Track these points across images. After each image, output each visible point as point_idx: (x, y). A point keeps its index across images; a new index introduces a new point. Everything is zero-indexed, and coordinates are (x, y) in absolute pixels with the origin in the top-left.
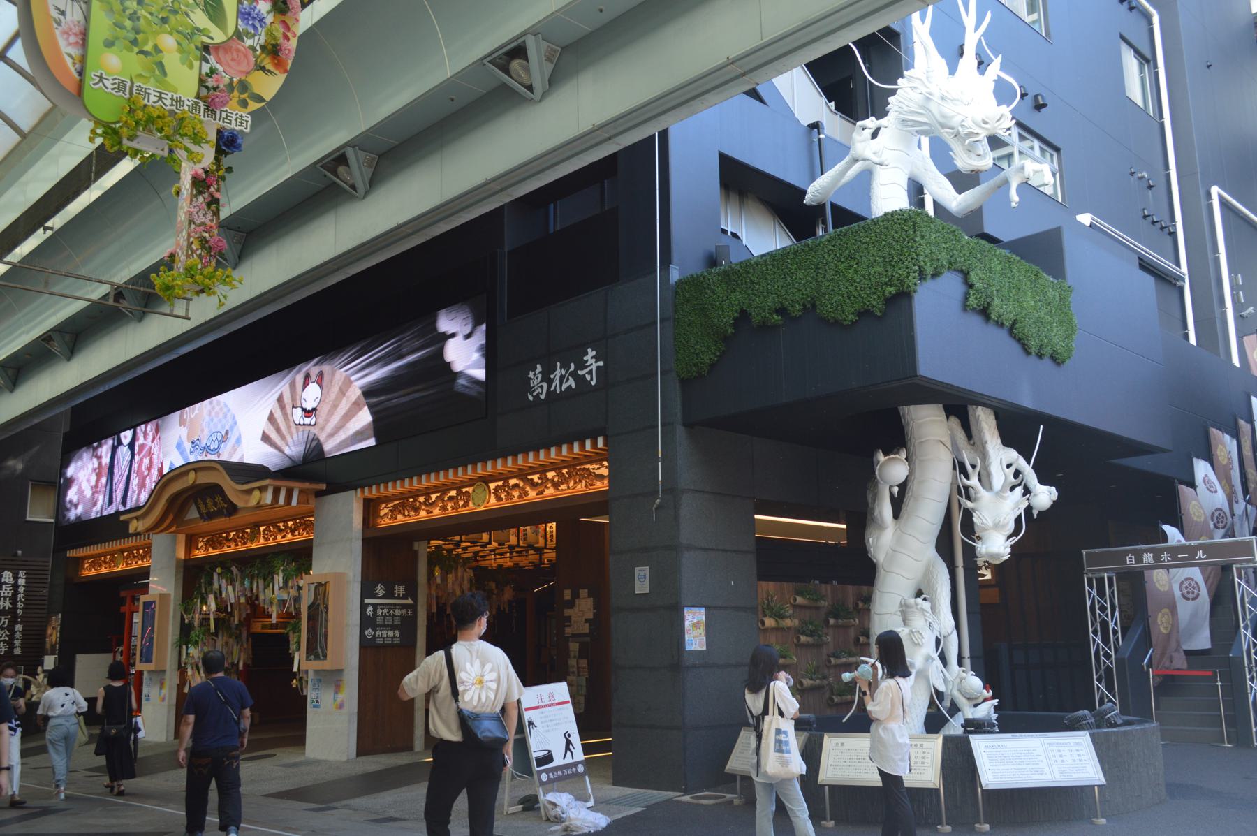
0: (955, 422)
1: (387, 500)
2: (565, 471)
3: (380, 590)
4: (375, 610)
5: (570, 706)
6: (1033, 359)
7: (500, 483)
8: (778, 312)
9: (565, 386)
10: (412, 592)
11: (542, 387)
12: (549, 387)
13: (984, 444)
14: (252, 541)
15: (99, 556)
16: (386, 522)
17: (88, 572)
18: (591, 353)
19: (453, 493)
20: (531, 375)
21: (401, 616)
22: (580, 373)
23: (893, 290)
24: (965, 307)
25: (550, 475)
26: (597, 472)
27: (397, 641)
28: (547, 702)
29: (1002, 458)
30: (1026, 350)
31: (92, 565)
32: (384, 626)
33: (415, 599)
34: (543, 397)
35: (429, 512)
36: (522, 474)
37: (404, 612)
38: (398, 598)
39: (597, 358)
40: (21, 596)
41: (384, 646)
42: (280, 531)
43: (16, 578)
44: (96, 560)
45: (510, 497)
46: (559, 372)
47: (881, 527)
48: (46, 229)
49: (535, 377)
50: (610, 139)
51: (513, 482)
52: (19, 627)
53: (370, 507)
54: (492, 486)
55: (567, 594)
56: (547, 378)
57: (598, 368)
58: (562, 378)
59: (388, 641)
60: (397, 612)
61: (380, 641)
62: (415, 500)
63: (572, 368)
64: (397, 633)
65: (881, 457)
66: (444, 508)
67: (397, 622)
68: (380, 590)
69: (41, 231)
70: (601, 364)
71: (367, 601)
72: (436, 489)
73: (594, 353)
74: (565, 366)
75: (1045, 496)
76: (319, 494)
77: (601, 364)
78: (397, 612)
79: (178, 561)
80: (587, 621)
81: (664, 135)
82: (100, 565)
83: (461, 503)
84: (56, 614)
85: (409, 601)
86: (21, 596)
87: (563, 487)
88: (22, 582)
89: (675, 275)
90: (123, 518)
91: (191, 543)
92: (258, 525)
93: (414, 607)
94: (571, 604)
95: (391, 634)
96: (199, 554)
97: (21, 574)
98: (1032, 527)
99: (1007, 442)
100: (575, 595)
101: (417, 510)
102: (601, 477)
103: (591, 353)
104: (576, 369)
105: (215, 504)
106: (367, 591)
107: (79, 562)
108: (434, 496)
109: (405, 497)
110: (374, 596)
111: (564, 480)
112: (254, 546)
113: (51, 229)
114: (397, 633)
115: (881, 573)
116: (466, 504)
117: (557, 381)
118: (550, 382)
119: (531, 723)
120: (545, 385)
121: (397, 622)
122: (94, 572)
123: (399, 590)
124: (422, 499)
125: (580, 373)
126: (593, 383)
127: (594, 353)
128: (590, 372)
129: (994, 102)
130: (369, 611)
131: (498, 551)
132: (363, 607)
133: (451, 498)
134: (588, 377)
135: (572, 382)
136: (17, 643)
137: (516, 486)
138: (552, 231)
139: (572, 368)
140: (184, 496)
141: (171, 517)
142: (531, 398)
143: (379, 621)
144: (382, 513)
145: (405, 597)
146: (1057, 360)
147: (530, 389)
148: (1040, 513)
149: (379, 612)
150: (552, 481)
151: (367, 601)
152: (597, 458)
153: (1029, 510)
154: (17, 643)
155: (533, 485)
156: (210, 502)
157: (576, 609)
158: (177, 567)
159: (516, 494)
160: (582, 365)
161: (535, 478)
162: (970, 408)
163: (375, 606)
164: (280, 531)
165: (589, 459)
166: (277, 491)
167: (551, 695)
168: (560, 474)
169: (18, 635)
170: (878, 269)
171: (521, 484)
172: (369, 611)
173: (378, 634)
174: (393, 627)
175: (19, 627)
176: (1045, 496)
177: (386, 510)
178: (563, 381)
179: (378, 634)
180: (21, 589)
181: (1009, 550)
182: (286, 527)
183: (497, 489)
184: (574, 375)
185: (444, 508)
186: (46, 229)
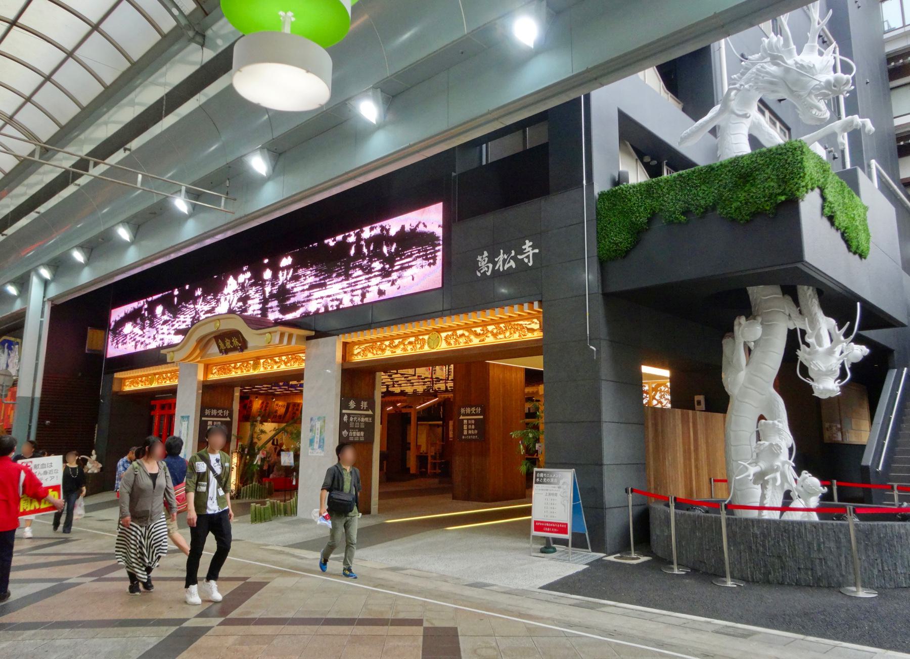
0: (788, 299)
1: (360, 343)
2: (502, 325)
3: (352, 404)
4: (349, 418)
6: (851, 254)
7: (450, 333)
8: (683, 213)
9: (506, 266)
10: (371, 406)
11: (488, 267)
12: (494, 267)
15: (138, 377)
16: (358, 359)
19: (412, 339)
20: (479, 258)
21: (365, 423)
22: (520, 257)
23: (783, 198)
24: (822, 214)
26: (529, 327)
27: (362, 439)
30: (849, 247)
31: (132, 383)
32: (354, 428)
33: (374, 411)
34: (489, 274)
35: (393, 352)
36: (467, 327)
37: (367, 419)
38: (363, 410)
39: (533, 247)
42: (276, 363)
44: (135, 380)
46: (502, 256)
47: (739, 370)
48: (125, 150)
49: (483, 260)
50: (596, 79)
51: (459, 332)
54: (444, 335)
56: (492, 260)
57: (534, 254)
58: (504, 261)
59: (357, 439)
60: (363, 420)
61: (351, 439)
62: (382, 344)
64: (362, 434)
66: (405, 349)
67: (363, 426)
68: (352, 404)
69: (122, 150)
70: (537, 251)
71: (344, 411)
73: (531, 243)
76: (309, 338)
77: (537, 251)
78: (363, 420)
79: (199, 382)
81: (587, 98)
83: (419, 346)
85: (370, 412)
87: (502, 336)
89: (597, 190)
90: (162, 352)
91: (207, 369)
92: (258, 358)
95: (358, 434)
96: (214, 376)
101: (383, 350)
104: (516, 254)
105: (232, 343)
106: (344, 405)
107: (122, 381)
108: (397, 342)
109: (374, 341)
110: (348, 408)
112: (256, 372)
113: (129, 150)
114: (362, 434)
115: (731, 400)
117: (501, 263)
118: (495, 264)
120: (491, 266)
121: (363, 426)
122: (132, 388)
123: (364, 404)
124: (387, 343)
125: (520, 257)
127: (531, 243)
128: (528, 257)
129: (688, 119)
130: (345, 418)
131: (410, 383)
132: (342, 415)
133: (410, 343)
134: (526, 260)
137: (463, 335)
138: (484, 163)
140: (207, 339)
141: (198, 351)
142: (479, 274)
143: (351, 425)
144: (356, 352)
145: (367, 410)
146: (861, 256)
149: (351, 419)
150: (492, 332)
151: (344, 411)
152: (530, 317)
155: (477, 335)
159: (462, 340)
160: (522, 252)
161: (478, 330)
163: (349, 415)
164: (276, 363)
165: (521, 318)
166: (282, 335)
168: (288, 358)
170: (772, 184)
171: (467, 334)
172: (345, 418)
173: (351, 434)
174: (360, 430)
177: (359, 350)
179: (351, 434)
182: (281, 360)
183: (446, 337)
184: (514, 258)
185: (405, 349)
186: (125, 150)
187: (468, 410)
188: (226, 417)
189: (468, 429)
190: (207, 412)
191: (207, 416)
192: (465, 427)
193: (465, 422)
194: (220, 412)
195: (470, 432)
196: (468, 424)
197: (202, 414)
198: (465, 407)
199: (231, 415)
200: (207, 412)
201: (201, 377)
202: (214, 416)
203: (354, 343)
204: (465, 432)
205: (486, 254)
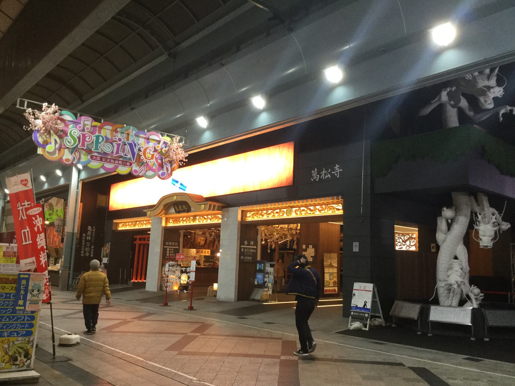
1: (250, 211)
4: (244, 250)
5: (354, 288)
7: (297, 209)
9: (326, 177)
12: (320, 177)
13: (483, 206)
14: (193, 221)
17: (121, 228)
18: (337, 166)
19: (278, 211)
20: (313, 172)
21: (253, 252)
22: (333, 173)
25: (318, 207)
28: (362, 289)
29: (489, 210)
33: (257, 246)
34: (317, 180)
36: (306, 206)
39: (340, 168)
40: (94, 235)
41: (247, 262)
42: (205, 219)
43: (92, 229)
45: (301, 213)
46: (324, 172)
49: (314, 173)
51: (302, 208)
52: (93, 247)
53: (244, 213)
54: (294, 209)
55: (304, 247)
56: (319, 173)
58: (325, 174)
59: (248, 261)
60: (251, 251)
61: (245, 261)
63: (330, 171)
65: (445, 209)
70: (341, 170)
72: (271, 209)
74: (327, 170)
75: (506, 226)
77: (341, 170)
79: (163, 227)
80: (311, 257)
82: (126, 226)
83: (281, 214)
84: (108, 243)
85: (255, 247)
86: (94, 235)
88: (94, 230)
93: (256, 249)
94: (305, 250)
95: (249, 258)
97: (94, 227)
98: (500, 237)
99: (492, 205)
100: (307, 247)
101: (263, 215)
102: (338, 210)
103: (337, 166)
105: (182, 208)
107: (117, 224)
108: (270, 211)
110: (244, 245)
111: (323, 210)
114: (251, 258)
116: (283, 215)
118: (320, 175)
119: (354, 294)
120: (318, 176)
122: (123, 228)
123: (252, 243)
125: (333, 173)
126: (338, 177)
133: (277, 213)
134: (336, 175)
135: (329, 176)
136: (92, 252)
137: (304, 210)
139: (330, 171)
142: (312, 180)
143: (245, 254)
145: (253, 246)
147: (313, 177)
148: (503, 232)
149: (245, 250)
153: (499, 230)
154: (92, 252)
155: (311, 210)
156: (180, 207)
157: (307, 252)
158: (162, 229)
159: (303, 213)
160: (334, 170)
161: (312, 208)
162: (478, 194)
163: (244, 248)
164: (205, 219)
167: (365, 287)
169: (92, 250)
171: (306, 209)
173: (245, 258)
174: (250, 256)
175: (93, 247)
176: (506, 226)
178: (325, 175)
179: (245, 258)
180: (94, 233)
181: (492, 245)
183: (296, 211)
184: (330, 173)
187: (170, 243)
188: (176, 246)
189: (169, 253)
190: (167, 243)
191: (167, 246)
192: (168, 252)
193: (168, 249)
194: (173, 243)
195: (171, 255)
196: (170, 251)
197: (164, 244)
198: (169, 242)
199: (179, 245)
200: (167, 243)
201: (164, 224)
202: (170, 246)
203: (247, 211)
204: (168, 255)
205: (316, 170)
